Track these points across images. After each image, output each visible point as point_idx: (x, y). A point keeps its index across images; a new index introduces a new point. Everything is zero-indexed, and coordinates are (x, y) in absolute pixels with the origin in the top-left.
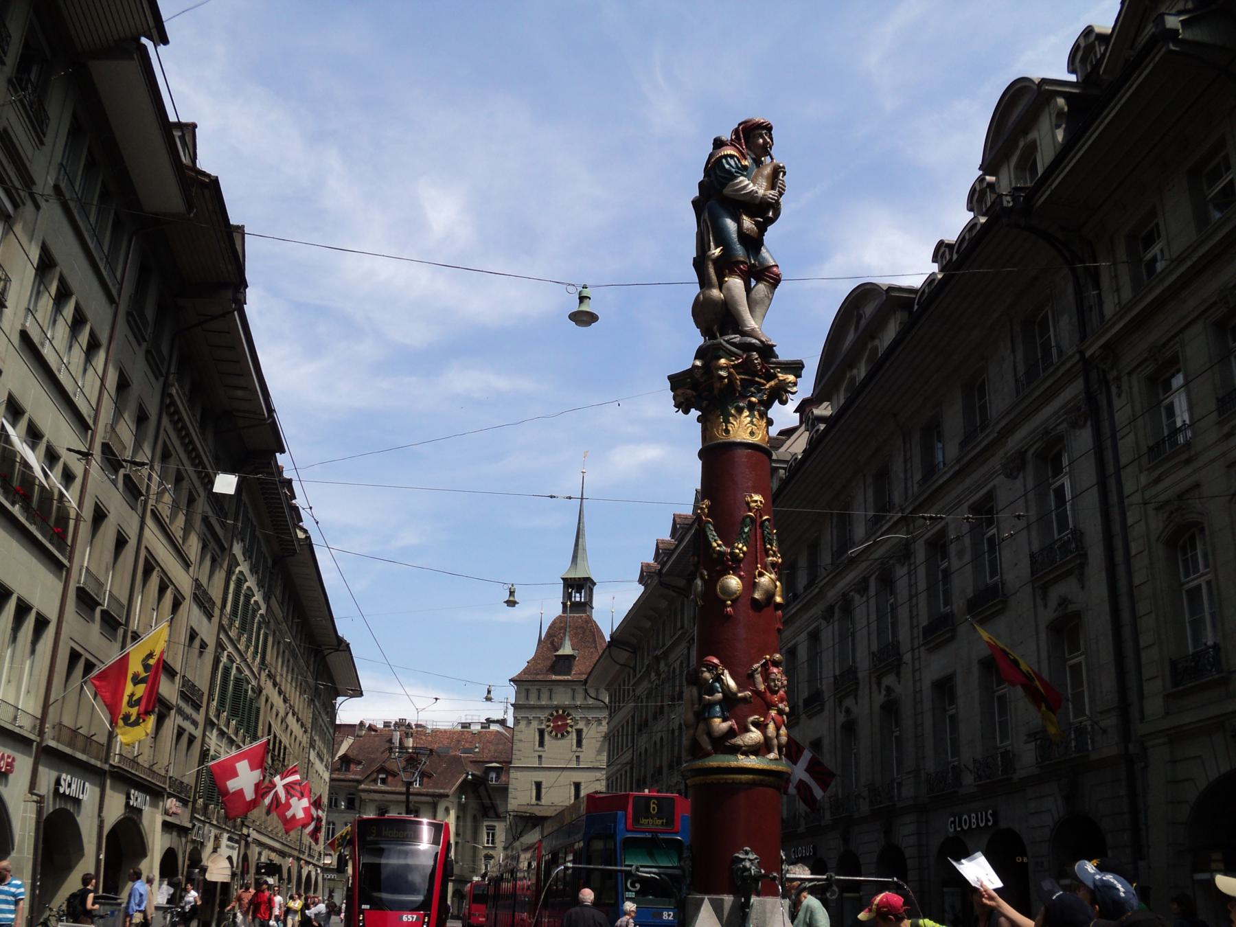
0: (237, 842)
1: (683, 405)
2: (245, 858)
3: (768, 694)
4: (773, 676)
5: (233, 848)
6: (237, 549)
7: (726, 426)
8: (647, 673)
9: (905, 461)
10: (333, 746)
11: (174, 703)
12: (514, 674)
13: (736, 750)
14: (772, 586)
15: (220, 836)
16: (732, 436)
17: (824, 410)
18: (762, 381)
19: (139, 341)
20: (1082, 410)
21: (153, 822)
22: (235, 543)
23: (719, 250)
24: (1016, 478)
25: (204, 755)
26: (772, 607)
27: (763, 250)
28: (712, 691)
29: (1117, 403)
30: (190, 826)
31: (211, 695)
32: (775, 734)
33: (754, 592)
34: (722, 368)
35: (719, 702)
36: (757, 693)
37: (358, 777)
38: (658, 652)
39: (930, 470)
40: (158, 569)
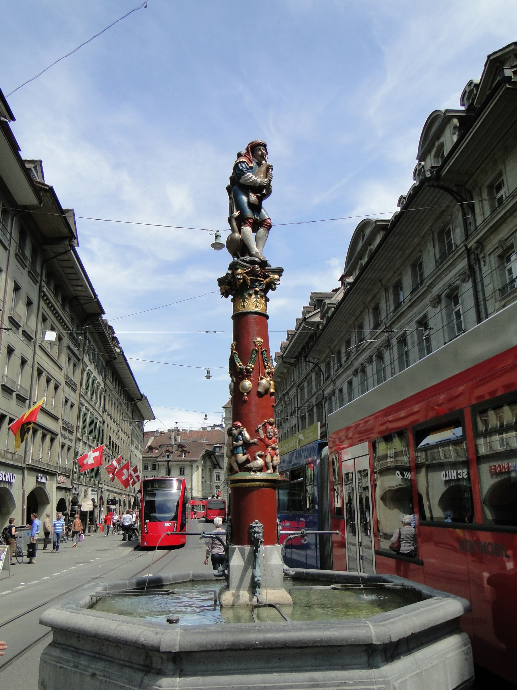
0: (96, 491)
1: (225, 294)
2: (101, 498)
3: (267, 440)
4: (268, 431)
5: (95, 494)
6: (86, 359)
7: (244, 304)
8: (280, 401)
9: (386, 302)
10: (143, 443)
11: (59, 432)
12: (224, 404)
13: (249, 470)
14: (268, 385)
15: (87, 490)
16: (246, 308)
17: (350, 280)
18: (262, 279)
19: (24, 266)
20: (467, 273)
21: (52, 487)
22: (85, 356)
23: (238, 213)
24: (436, 308)
25: (76, 454)
26: (268, 395)
27: (262, 210)
28: (237, 440)
29: (484, 269)
30: (71, 487)
31: (78, 426)
32: (271, 460)
33: (258, 388)
34: (239, 274)
35: (241, 446)
36: (261, 440)
37: (157, 455)
38: (284, 392)
39: (398, 305)
40: (45, 372)
